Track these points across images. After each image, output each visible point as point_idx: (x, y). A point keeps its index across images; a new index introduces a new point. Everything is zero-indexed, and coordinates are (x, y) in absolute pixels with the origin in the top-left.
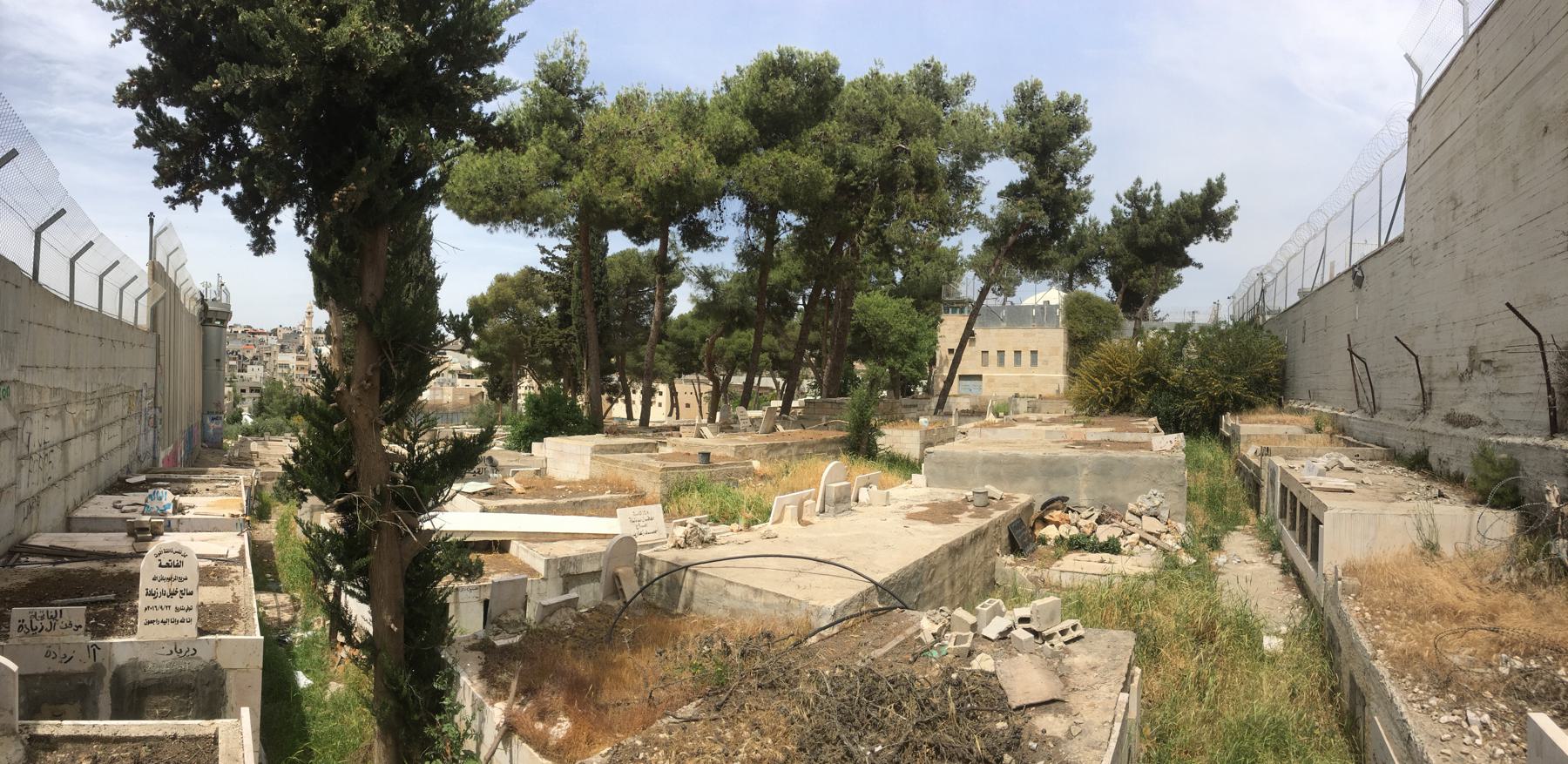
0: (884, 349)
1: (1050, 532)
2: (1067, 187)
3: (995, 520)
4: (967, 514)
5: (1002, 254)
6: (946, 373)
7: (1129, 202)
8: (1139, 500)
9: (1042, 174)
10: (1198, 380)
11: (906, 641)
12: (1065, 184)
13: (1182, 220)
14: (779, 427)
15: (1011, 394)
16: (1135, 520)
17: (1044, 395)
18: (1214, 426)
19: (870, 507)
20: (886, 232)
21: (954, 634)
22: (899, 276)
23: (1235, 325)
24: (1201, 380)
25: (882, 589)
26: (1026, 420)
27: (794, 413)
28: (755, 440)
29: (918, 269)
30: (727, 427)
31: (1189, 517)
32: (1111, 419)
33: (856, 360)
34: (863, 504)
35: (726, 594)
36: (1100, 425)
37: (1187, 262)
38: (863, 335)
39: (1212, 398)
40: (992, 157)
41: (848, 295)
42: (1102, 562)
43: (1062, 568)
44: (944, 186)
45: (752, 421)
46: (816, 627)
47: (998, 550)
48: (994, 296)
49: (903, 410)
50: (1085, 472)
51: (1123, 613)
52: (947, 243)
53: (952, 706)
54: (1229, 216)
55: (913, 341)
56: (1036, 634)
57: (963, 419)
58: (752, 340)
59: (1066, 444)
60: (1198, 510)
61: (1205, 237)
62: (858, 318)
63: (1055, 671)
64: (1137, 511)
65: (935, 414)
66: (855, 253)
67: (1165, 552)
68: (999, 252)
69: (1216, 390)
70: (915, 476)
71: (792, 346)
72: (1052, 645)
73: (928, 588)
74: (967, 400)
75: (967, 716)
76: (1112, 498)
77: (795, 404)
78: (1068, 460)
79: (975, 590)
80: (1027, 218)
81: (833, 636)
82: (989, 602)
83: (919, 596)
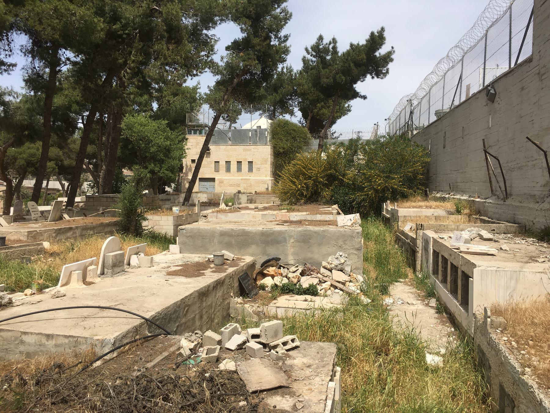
0: (146, 157)
1: (268, 281)
2: (272, 43)
3: (230, 273)
4: (210, 270)
5: (229, 92)
6: (190, 177)
7: (314, 54)
8: (330, 259)
9: (256, 34)
10: (366, 179)
11: (170, 355)
12: (271, 41)
13: (352, 65)
14: (66, 216)
15: (235, 191)
16: (327, 273)
17: (258, 191)
18: (378, 211)
19: (139, 269)
20: (146, 71)
21: (206, 348)
22: (155, 106)
23: (391, 138)
24: (368, 178)
25: (150, 322)
26: (247, 208)
27: (78, 206)
28: (45, 227)
29: (169, 101)
30: (20, 218)
31: (365, 272)
32: (305, 207)
33: (124, 167)
34: (134, 267)
35: (22, 342)
36: (298, 211)
37: (355, 95)
38: (130, 147)
39: (376, 191)
40: (222, 20)
41: (118, 117)
42: (306, 300)
43: (277, 305)
44: (187, 39)
45: (42, 212)
46: (100, 354)
47: (232, 294)
48: (223, 121)
49: (161, 203)
50: (292, 240)
51: (323, 334)
52: (190, 83)
53: (208, 393)
54: (387, 58)
55: (167, 151)
56: (265, 345)
57: (203, 208)
58: (41, 151)
59: (278, 222)
60: (371, 267)
61: (369, 76)
62: (125, 134)
63: (281, 368)
64: (329, 267)
65: (183, 205)
66: (122, 85)
67: (349, 294)
68: (227, 90)
69: (379, 185)
70: (171, 246)
71: (74, 156)
72: (277, 352)
73: (183, 320)
74: (205, 195)
75: (219, 399)
76: (311, 258)
77: (77, 199)
78: (280, 233)
79: (216, 321)
80: (246, 66)
81: (113, 359)
82: (230, 326)
83: (178, 327)
